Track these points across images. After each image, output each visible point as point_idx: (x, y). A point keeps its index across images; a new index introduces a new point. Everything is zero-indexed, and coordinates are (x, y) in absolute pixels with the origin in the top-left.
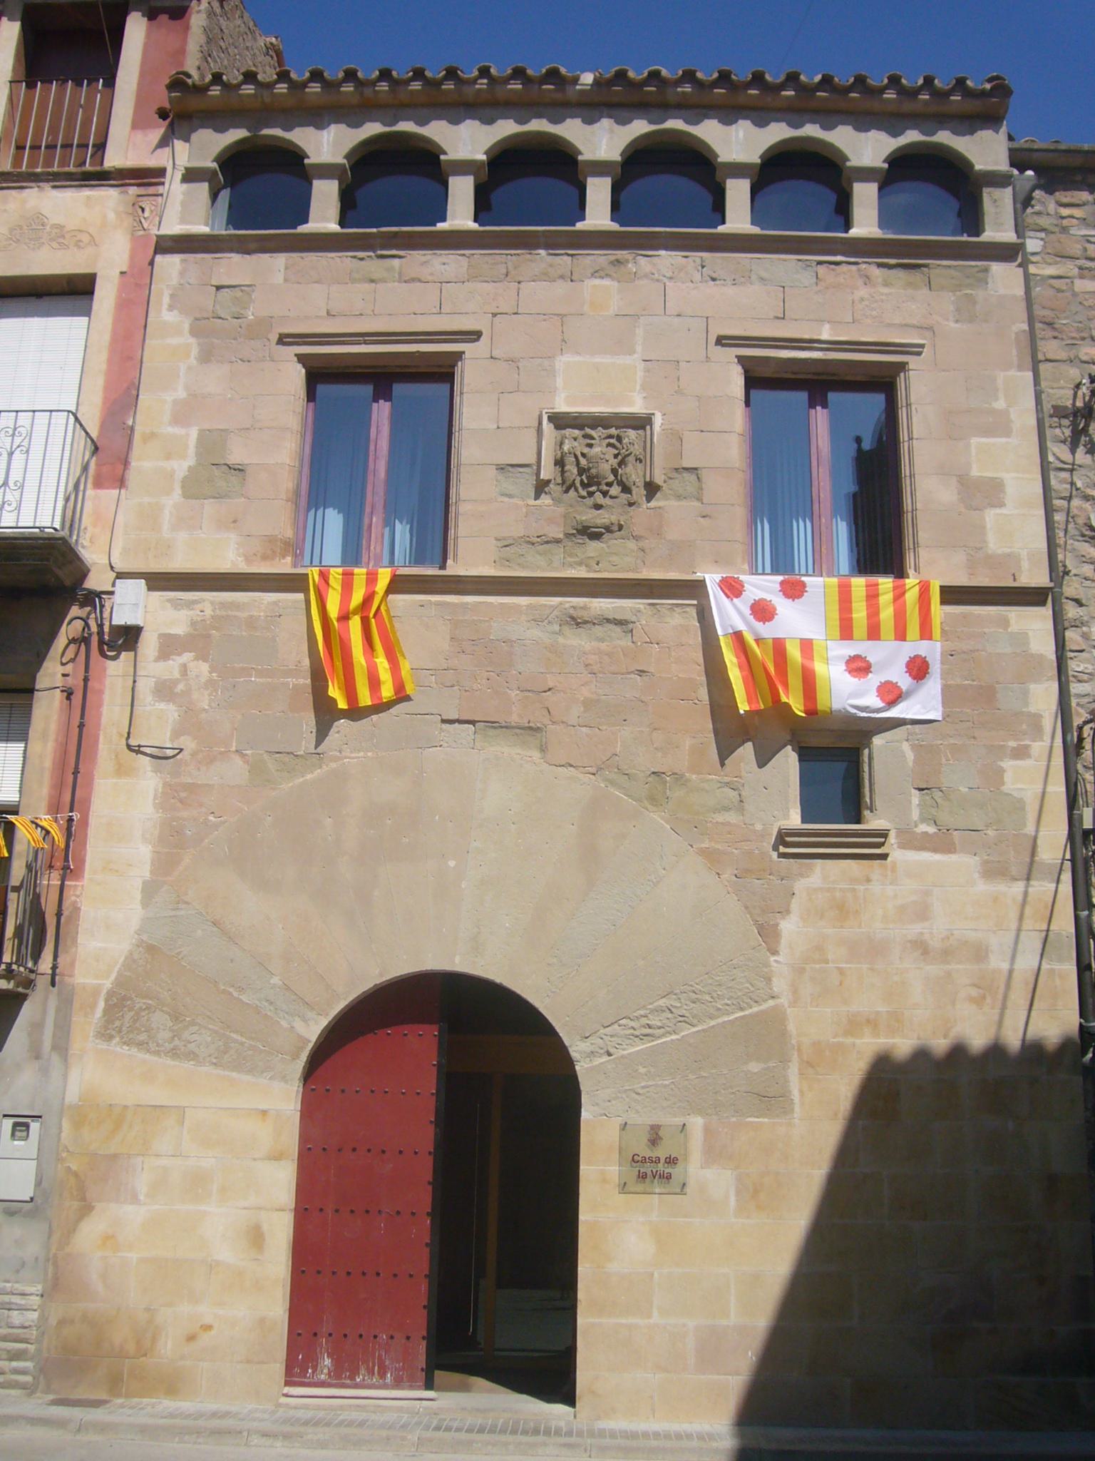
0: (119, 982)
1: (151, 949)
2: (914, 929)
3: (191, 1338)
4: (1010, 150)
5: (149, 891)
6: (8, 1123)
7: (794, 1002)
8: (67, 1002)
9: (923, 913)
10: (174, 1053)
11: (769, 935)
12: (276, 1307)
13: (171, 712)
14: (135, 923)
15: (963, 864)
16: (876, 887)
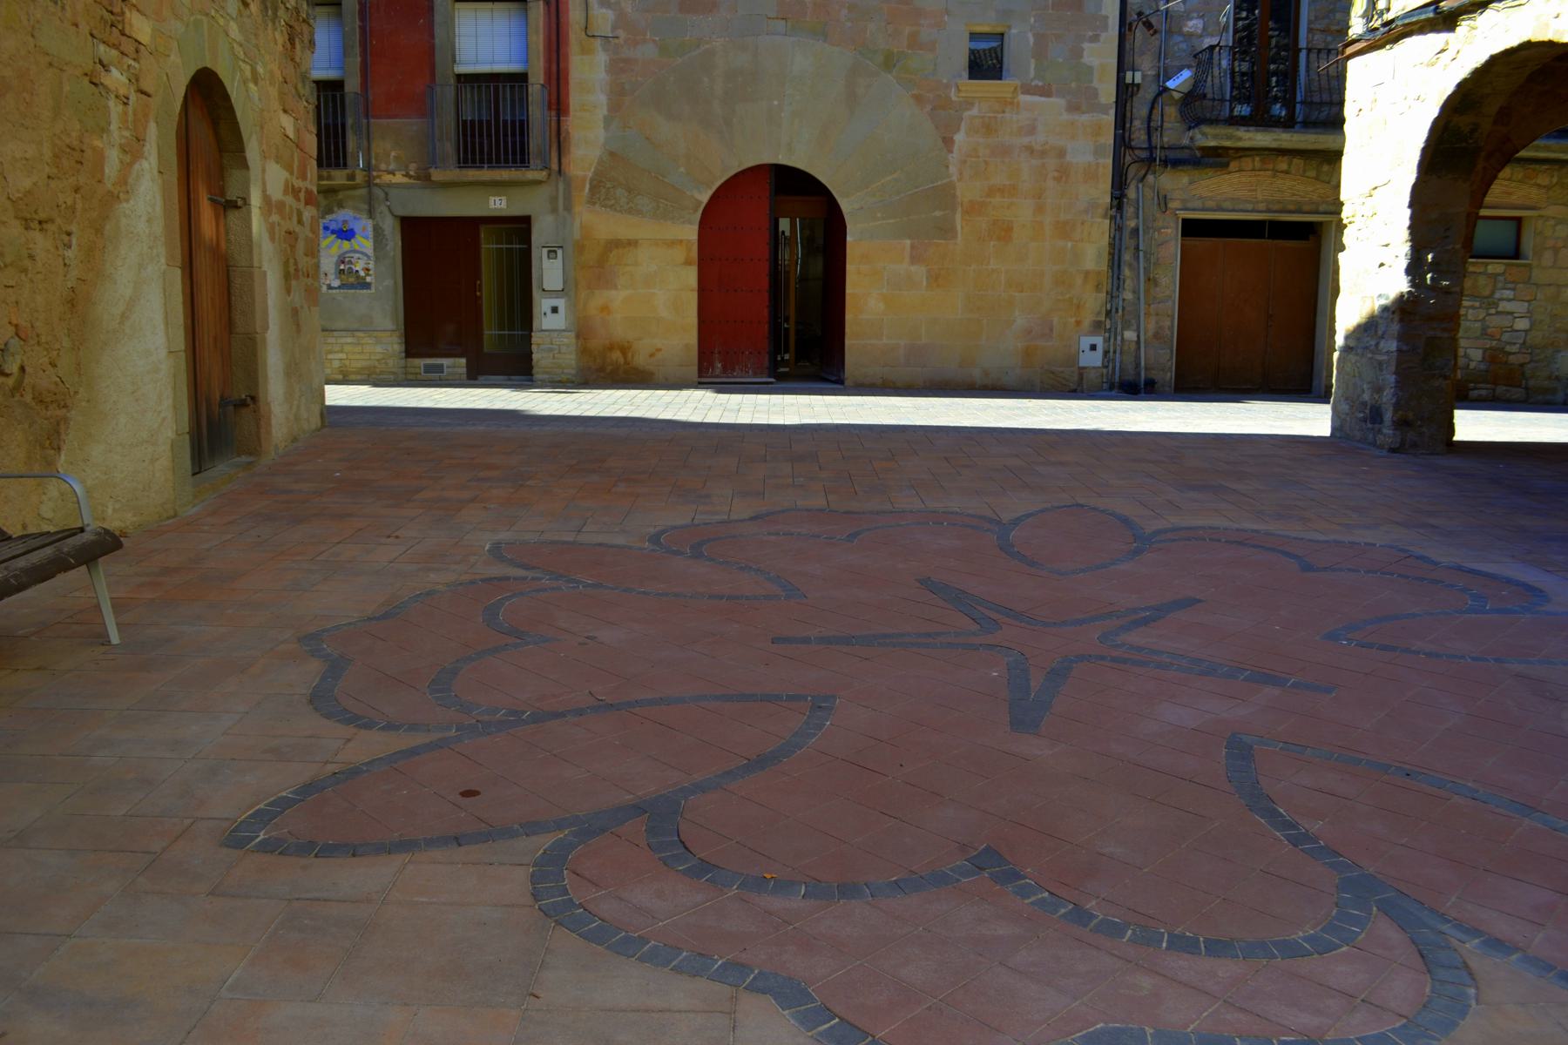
0: (596, 173)
1: (612, 154)
2: (1025, 140)
3: (652, 355)
4: (972, 52)
5: (608, 121)
6: (545, 251)
7: (960, 180)
8: (568, 185)
9: (1032, 130)
10: (630, 211)
11: (948, 142)
12: (692, 338)
13: (610, 15)
14: (602, 140)
15: (1058, 102)
16: (1007, 115)
